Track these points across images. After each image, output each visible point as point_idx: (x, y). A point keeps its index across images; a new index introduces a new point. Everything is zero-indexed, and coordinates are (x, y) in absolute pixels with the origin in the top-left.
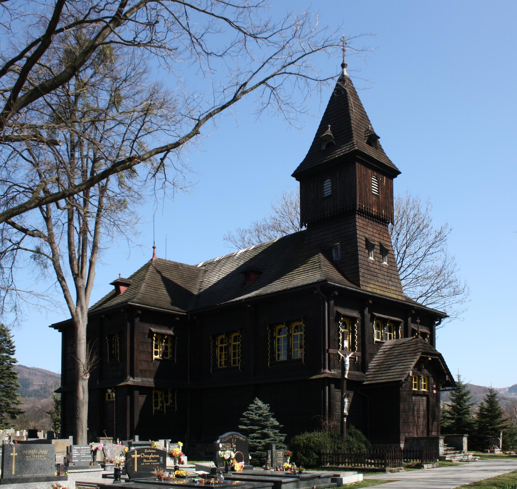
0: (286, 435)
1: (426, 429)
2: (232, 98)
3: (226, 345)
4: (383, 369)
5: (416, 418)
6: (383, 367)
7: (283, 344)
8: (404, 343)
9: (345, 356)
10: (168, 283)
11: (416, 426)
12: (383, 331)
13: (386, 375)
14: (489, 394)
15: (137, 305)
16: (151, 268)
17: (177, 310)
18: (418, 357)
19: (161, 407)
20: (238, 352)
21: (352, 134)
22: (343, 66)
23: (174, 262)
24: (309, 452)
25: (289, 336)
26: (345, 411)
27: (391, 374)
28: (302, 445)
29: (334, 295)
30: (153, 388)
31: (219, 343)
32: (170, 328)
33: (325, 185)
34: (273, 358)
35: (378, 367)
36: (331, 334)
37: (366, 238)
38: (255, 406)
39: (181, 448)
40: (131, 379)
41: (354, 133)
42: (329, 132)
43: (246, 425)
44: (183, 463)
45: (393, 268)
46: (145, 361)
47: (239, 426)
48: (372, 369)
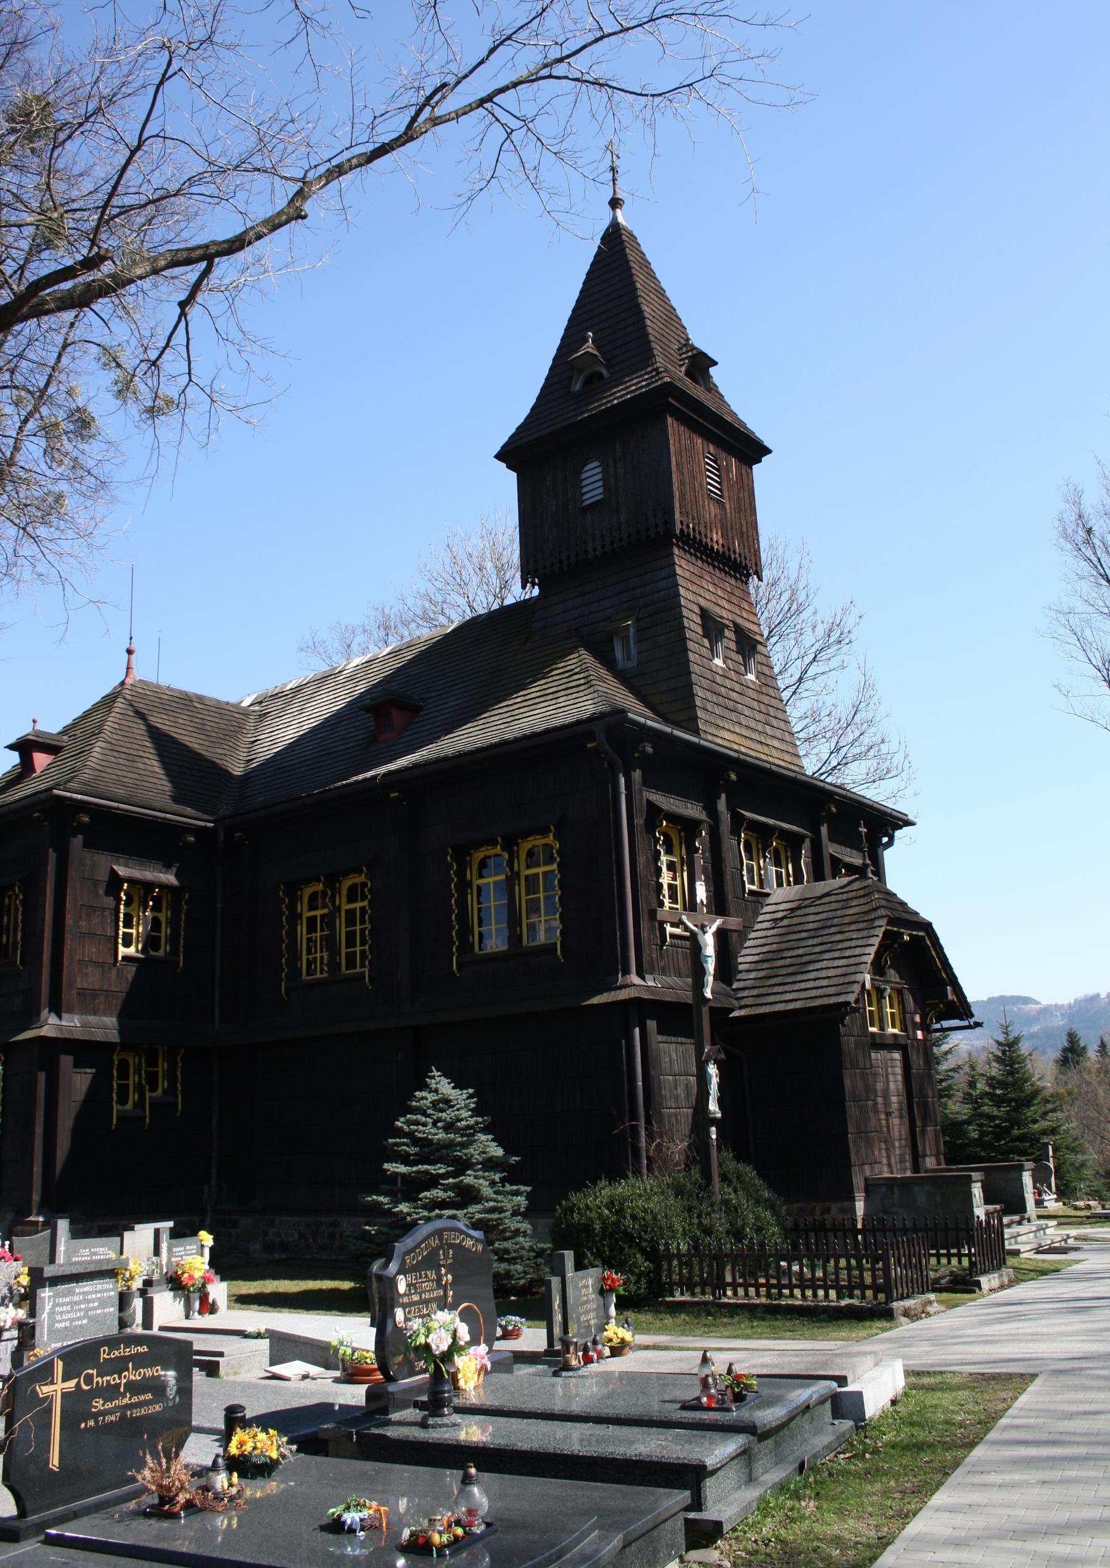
0: (529, 1189)
1: (908, 1151)
2: (403, 129)
3: (326, 911)
4: (784, 971)
5: (883, 1116)
6: (780, 963)
7: (494, 903)
8: (827, 894)
9: (703, 928)
10: (165, 745)
11: (885, 1142)
12: (761, 861)
13: (796, 987)
14: (1001, 1038)
15: (80, 797)
16: (120, 704)
17: (189, 816)
18: (880, 932)
19: (135, 1104)
20: (362, 931)
21: (651, 350)
22: (615, 203)
23: (180, 692)
24: (622, 1249)
25: (513, 878)
26: (713, 1106)
27: (811, 984)
28: (597, 1226)
29: (644, 752)
30: (116, 1044)
31: (305, 907)
32: (168, 866)
33: (584, 476)
34: (466, 947)
35: (766, 965)
36: (640, 868)
37: (701, 608)
38: (431, 1097)
39: (207, 1252)
40: (53, 1019)
41: (657, 350)
42: (589, 347)
43: (405, 1159)
44: (212, 1309)
45: (771, 692)
46: (95, 963)
47: (386, 1166)
48: (748, 971)
